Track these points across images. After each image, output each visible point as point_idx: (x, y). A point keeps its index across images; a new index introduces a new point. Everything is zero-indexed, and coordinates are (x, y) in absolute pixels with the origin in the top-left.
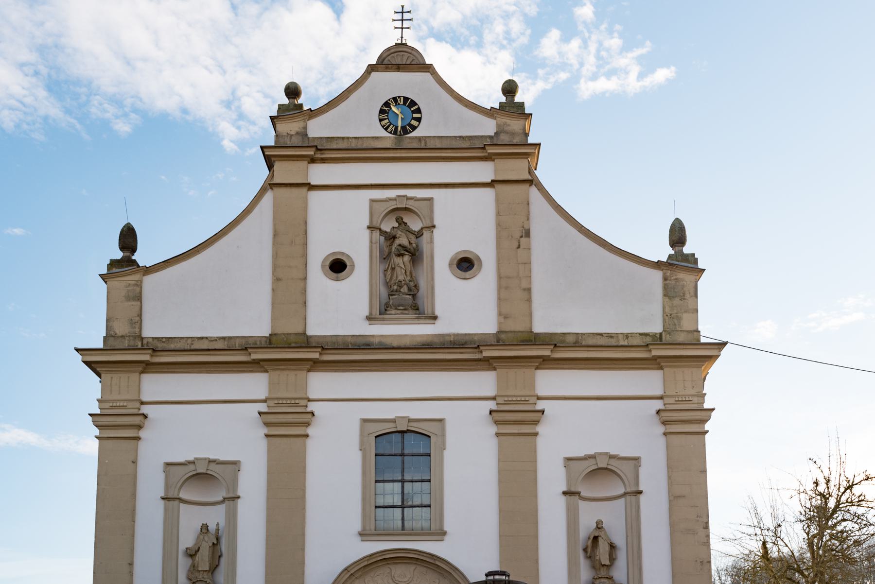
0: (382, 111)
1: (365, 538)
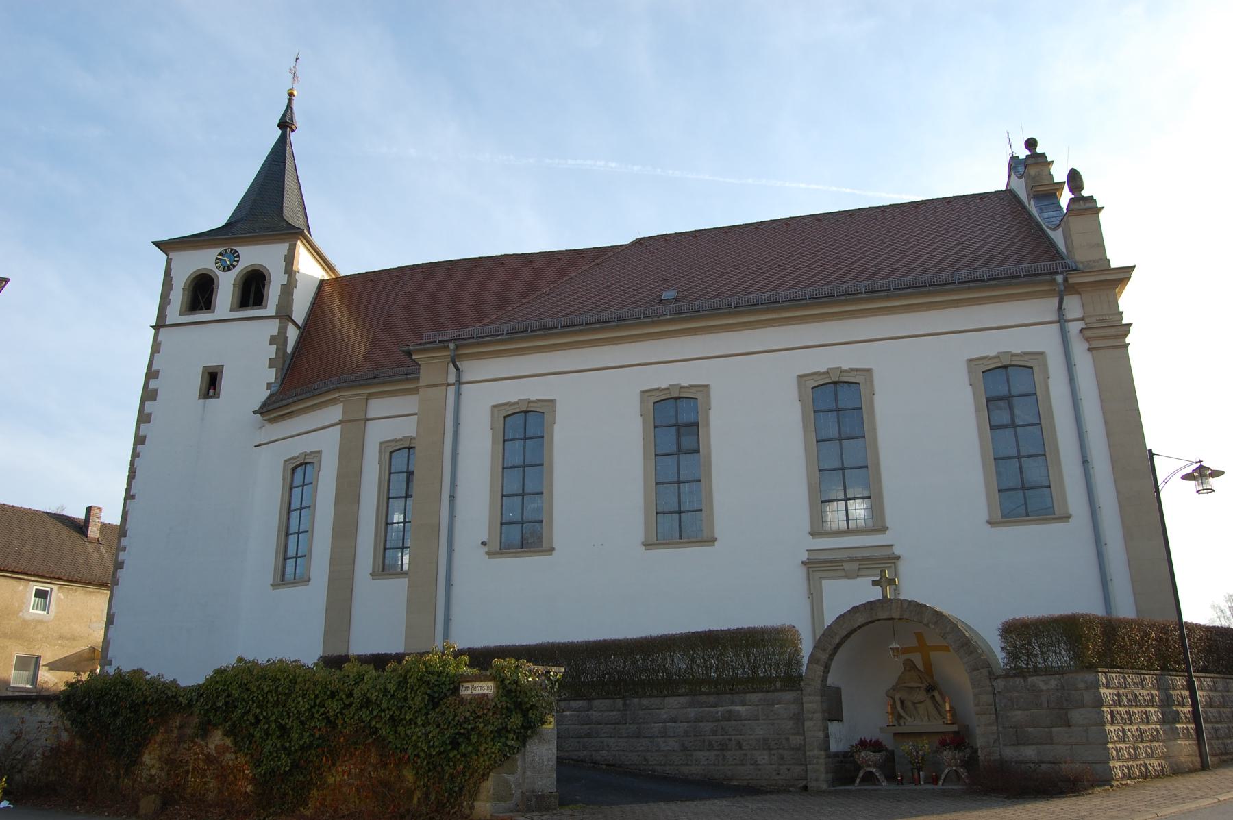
1: (648, 547)
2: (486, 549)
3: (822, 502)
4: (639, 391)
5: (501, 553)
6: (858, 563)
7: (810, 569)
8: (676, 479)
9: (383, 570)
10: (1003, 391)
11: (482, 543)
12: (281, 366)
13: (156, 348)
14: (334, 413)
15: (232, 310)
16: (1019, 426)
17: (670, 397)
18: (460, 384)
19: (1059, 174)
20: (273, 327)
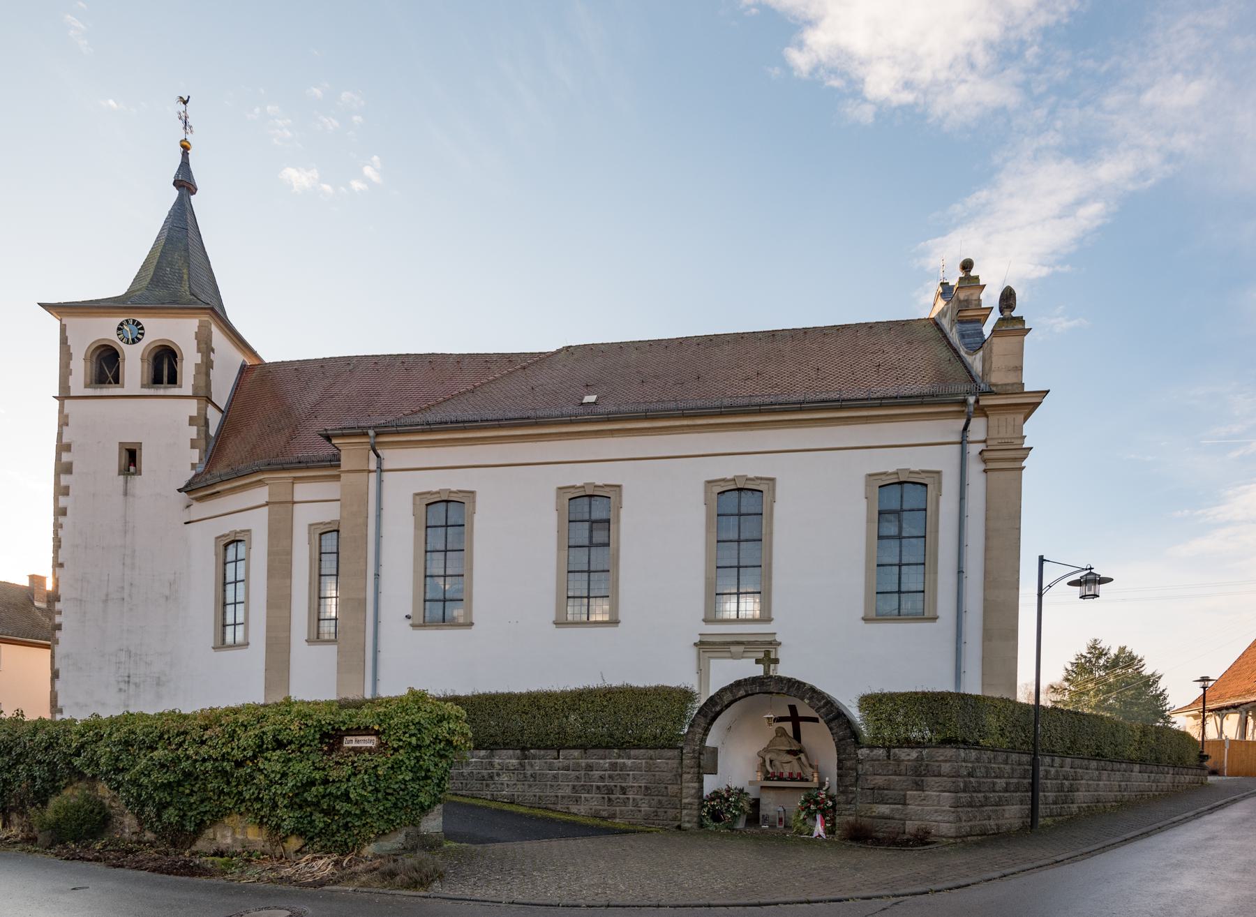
0: (119, 329)
2: (410, 621)
3: (717, 594)
4: (555, 488)
5: (425, 626)
6: (744, 647)
7: (701, 650)
8: (586, 568)
9: (318, 638)
10: (895, 505)
11: (406, 616)
12: (204, 447)
13: (64, 421)
14: (261, 495)
15: (143, 386)
16: (905, 538)
17: (584, 494)
18: (381, 471)
19: (990, 298)
20: (192, 407)
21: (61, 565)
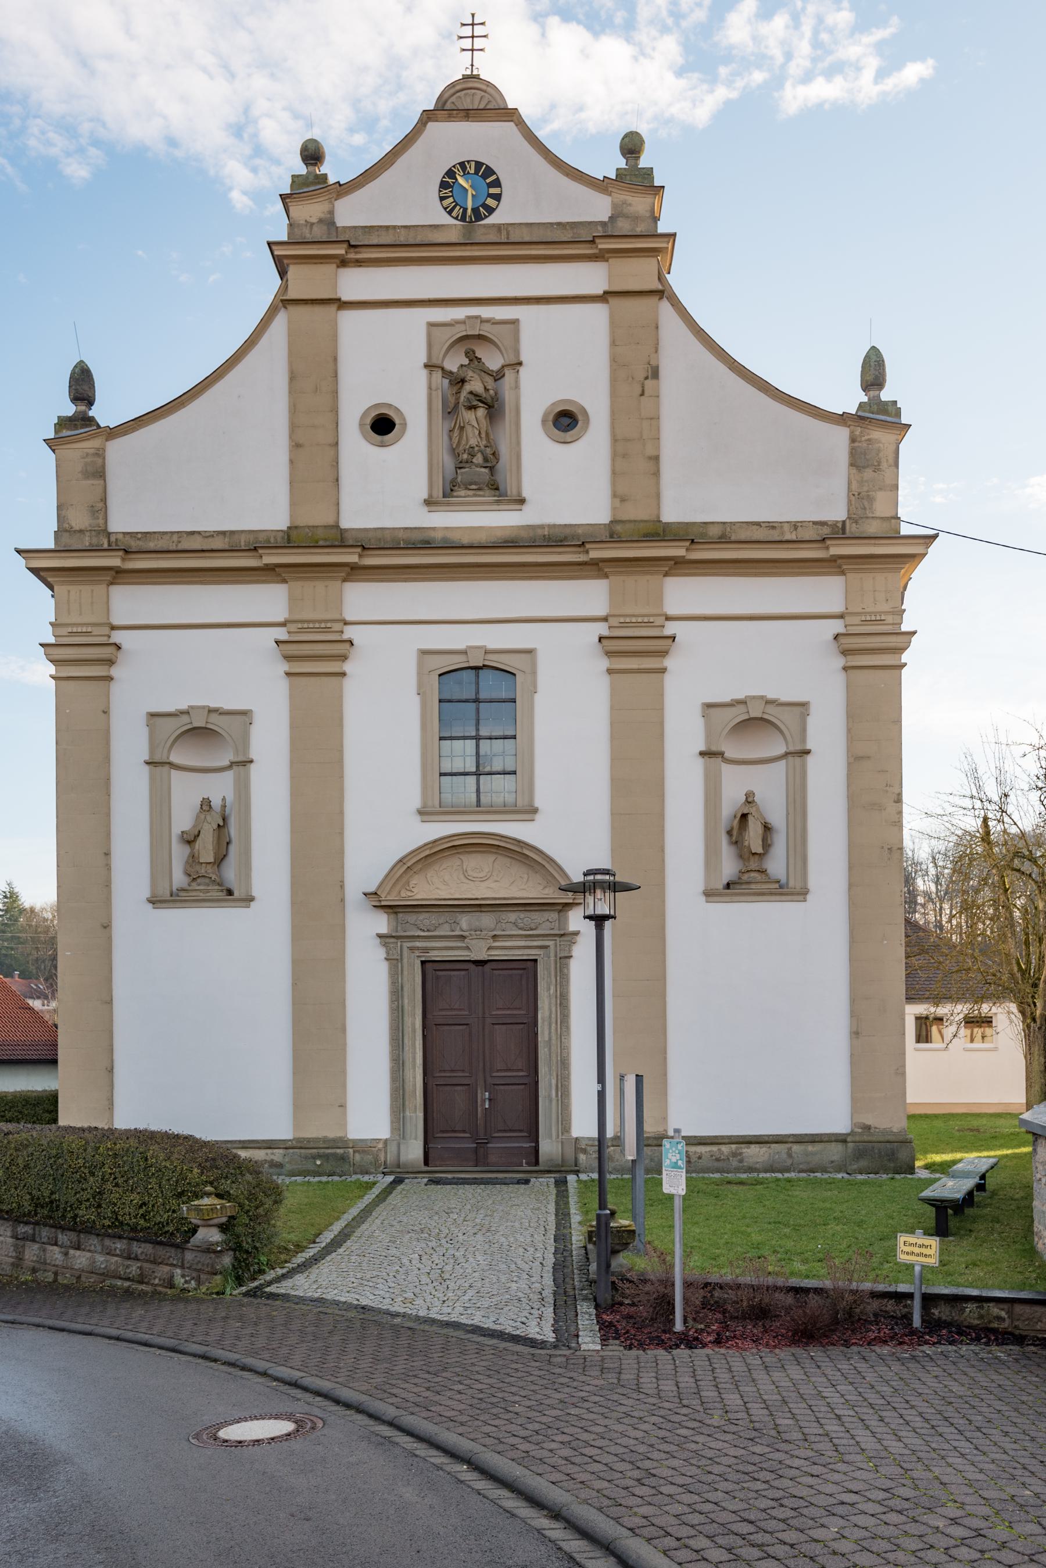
0: (443, 185)
21: (899, 849)
